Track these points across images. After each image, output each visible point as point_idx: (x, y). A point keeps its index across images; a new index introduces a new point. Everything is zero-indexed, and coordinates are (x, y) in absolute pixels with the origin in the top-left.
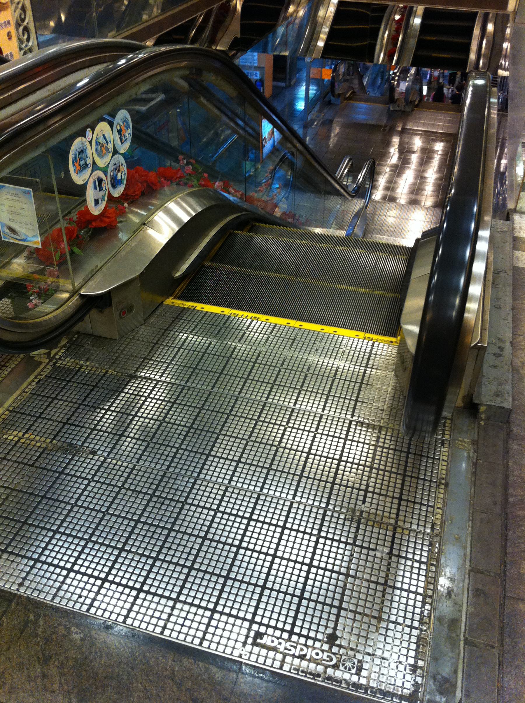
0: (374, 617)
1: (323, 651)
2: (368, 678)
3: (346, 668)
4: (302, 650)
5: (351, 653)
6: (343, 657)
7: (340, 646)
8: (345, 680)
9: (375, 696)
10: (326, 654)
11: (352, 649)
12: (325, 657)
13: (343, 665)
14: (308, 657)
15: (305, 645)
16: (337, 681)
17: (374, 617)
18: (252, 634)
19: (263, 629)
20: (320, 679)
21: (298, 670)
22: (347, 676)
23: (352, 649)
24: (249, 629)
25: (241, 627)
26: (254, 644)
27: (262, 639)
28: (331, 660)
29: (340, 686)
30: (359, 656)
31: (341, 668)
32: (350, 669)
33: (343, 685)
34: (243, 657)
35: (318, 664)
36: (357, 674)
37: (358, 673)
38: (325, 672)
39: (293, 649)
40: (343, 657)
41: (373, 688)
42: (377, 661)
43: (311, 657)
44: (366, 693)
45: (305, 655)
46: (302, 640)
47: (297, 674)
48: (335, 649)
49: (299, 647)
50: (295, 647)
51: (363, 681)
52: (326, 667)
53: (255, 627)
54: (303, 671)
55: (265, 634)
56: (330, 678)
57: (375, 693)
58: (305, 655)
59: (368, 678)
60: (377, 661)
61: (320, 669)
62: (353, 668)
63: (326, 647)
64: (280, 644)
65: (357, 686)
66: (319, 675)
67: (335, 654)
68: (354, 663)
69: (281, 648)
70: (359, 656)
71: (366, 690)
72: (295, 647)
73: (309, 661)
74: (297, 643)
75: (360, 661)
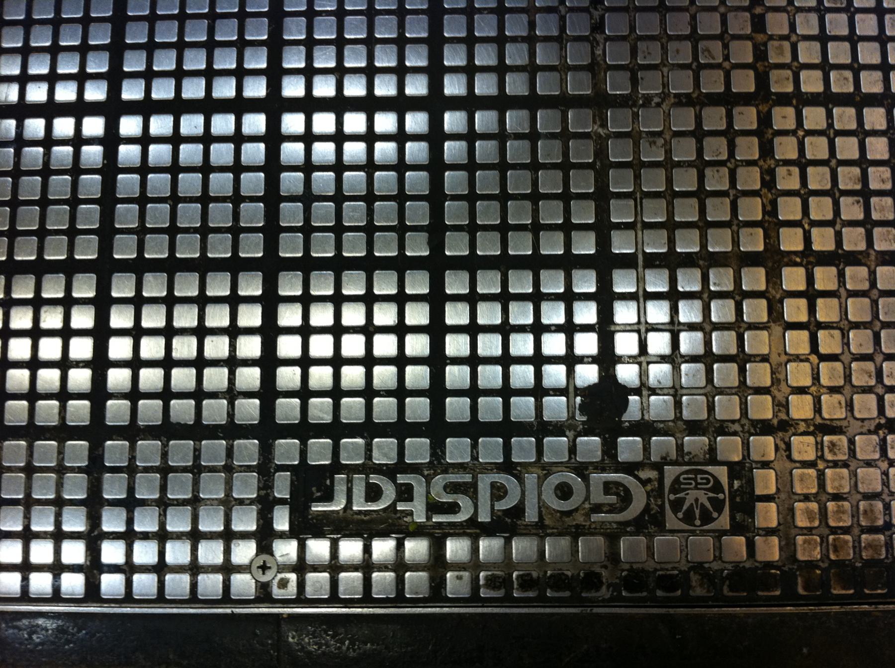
0: (578, 102)
1: (582, 470)
2: (785, 530)
3: (689, 518)
4: (498, 492)
5: (694, 443)
6: (671, 472)
7: (645, 429)
8: (698, 567)
9: (828, 599)
10: (598, 478)
11: (694, 428)
12: (597, 496)
13: (677, 505)
14: (531, 515)
15: (508, 466)
16: (668, 582)
17: (578, 102)
18: (282, 488)
19: (320, 451)
20: (604, 592)
21: (504, 582)
22: (702, 546)
23: (694, 428)
24: (266, 469)
25: (229, 469)
26: (304, 528)
27: (328, 497)
28: (626, 498)
29: (688, 601)
30: (730, 447)
31: (672, 521)
32: (707, 518)
33: (699, 592)
34: (277, 593)
35: (577, 532)
36: (737, 529)
37: (743, 525)
38: (613, 557)
39: (464, 501)
40: (671, 472)
41: (811, 565)
42: (803, 447)
43: (542, 506)
44: (790, 597)
45: (518, 510)
46: (491, 449)
47: (508, 600)
48: (629, 446)
49: (484, 483)
50: (470, 490)
51: (770, 550)
52: (613, 538)
53: (286, 449)
54: (526, 582)
55: (336, 467)
56: (636, 580)
57: (825, 585)
58: (518, 510)
59: (785, 530)
60: (803, 447)
61: (590, 549)
62: (718, 505)
63: (591, 445)
64: (405, 493)
65: (750, 579)
66: (592, 580)
67: (630, 468)
68: (717, 487)
69: (418, 511)
70: (730, 447)
71: (787, 580)
72: (470, 490)
73: (540, 530)
74: (474, 467)
75: (738, 470)
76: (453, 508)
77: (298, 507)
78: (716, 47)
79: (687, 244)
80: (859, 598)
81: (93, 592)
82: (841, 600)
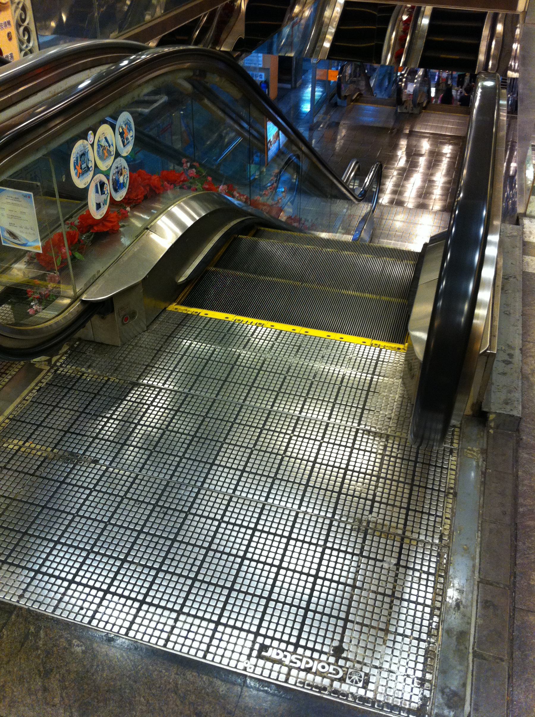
1: (329, 664)
2: (375, 692)
3: (352, 681)
4: (307, 663)
5: (358, 666)
6: (350, 671)
7: (347, 659)
8: (352, 693)
9: (382, 710)
10: (332, 667)
11: (358, 662)
12: (331, 670)
13: (350, 678)
14: (314, 670)
15: (311, 658)
16: (343, 695)
18: (257, 647)
19: (268, 642)
20: (326, 693)
21: (304, 683)
22: (353, 689)
23: (358, 662)
24: (254, 642)
25: (245, 639)
26: (259, 657)
27: (267, 651)
28: (338, 673)
29: (346, 700)
30: (366, 670)
31: (348, 681)
32: (356, 683)
33: (350, 699)
34: (248, 670)
35: (324, 677)
36: (363, 687)
37: (365, 687)
38: (331, 685)
39: (298, 662)
40: (350, 671)
41: (380, 701)
42: (385, 674)
43: (317, 670)
44: (373, 706)
45: (311, 668)
46: (308, 653)
47: (303, 687)
48: (341, 662)
49: (305, 660)
50: (301, 660)
51: (370, 695)
52: (333, 680)
53: (260, 639)
54: (309, 685)
55: (271, 646)
56: (336, 692)
57: (383, 707)
58: (311, 668)
59: (375, 692)
60: (385, 674)
61: (326, 682)
62: (360, 681)
63: (332, 660)
64: (285, 656)
65: (364, 700)
66: (325, 689)
67: (341, 667)
68: (361, 677)
69: (287, 661)
70: (366, 670)
71: (373, 703)
72: (301, 660)
73: (315, 674)
74: (303, 656)
75: (366, 674)
76: (297, 659)
77: (260, 651)
78: (384, 583)
79: (367, 622)
80: (363, 705)
81: (165, 646)
82: (358, 704)
